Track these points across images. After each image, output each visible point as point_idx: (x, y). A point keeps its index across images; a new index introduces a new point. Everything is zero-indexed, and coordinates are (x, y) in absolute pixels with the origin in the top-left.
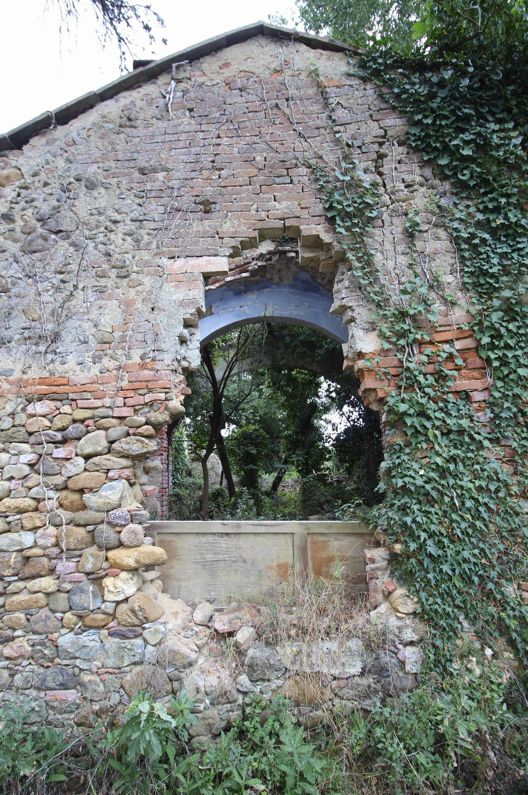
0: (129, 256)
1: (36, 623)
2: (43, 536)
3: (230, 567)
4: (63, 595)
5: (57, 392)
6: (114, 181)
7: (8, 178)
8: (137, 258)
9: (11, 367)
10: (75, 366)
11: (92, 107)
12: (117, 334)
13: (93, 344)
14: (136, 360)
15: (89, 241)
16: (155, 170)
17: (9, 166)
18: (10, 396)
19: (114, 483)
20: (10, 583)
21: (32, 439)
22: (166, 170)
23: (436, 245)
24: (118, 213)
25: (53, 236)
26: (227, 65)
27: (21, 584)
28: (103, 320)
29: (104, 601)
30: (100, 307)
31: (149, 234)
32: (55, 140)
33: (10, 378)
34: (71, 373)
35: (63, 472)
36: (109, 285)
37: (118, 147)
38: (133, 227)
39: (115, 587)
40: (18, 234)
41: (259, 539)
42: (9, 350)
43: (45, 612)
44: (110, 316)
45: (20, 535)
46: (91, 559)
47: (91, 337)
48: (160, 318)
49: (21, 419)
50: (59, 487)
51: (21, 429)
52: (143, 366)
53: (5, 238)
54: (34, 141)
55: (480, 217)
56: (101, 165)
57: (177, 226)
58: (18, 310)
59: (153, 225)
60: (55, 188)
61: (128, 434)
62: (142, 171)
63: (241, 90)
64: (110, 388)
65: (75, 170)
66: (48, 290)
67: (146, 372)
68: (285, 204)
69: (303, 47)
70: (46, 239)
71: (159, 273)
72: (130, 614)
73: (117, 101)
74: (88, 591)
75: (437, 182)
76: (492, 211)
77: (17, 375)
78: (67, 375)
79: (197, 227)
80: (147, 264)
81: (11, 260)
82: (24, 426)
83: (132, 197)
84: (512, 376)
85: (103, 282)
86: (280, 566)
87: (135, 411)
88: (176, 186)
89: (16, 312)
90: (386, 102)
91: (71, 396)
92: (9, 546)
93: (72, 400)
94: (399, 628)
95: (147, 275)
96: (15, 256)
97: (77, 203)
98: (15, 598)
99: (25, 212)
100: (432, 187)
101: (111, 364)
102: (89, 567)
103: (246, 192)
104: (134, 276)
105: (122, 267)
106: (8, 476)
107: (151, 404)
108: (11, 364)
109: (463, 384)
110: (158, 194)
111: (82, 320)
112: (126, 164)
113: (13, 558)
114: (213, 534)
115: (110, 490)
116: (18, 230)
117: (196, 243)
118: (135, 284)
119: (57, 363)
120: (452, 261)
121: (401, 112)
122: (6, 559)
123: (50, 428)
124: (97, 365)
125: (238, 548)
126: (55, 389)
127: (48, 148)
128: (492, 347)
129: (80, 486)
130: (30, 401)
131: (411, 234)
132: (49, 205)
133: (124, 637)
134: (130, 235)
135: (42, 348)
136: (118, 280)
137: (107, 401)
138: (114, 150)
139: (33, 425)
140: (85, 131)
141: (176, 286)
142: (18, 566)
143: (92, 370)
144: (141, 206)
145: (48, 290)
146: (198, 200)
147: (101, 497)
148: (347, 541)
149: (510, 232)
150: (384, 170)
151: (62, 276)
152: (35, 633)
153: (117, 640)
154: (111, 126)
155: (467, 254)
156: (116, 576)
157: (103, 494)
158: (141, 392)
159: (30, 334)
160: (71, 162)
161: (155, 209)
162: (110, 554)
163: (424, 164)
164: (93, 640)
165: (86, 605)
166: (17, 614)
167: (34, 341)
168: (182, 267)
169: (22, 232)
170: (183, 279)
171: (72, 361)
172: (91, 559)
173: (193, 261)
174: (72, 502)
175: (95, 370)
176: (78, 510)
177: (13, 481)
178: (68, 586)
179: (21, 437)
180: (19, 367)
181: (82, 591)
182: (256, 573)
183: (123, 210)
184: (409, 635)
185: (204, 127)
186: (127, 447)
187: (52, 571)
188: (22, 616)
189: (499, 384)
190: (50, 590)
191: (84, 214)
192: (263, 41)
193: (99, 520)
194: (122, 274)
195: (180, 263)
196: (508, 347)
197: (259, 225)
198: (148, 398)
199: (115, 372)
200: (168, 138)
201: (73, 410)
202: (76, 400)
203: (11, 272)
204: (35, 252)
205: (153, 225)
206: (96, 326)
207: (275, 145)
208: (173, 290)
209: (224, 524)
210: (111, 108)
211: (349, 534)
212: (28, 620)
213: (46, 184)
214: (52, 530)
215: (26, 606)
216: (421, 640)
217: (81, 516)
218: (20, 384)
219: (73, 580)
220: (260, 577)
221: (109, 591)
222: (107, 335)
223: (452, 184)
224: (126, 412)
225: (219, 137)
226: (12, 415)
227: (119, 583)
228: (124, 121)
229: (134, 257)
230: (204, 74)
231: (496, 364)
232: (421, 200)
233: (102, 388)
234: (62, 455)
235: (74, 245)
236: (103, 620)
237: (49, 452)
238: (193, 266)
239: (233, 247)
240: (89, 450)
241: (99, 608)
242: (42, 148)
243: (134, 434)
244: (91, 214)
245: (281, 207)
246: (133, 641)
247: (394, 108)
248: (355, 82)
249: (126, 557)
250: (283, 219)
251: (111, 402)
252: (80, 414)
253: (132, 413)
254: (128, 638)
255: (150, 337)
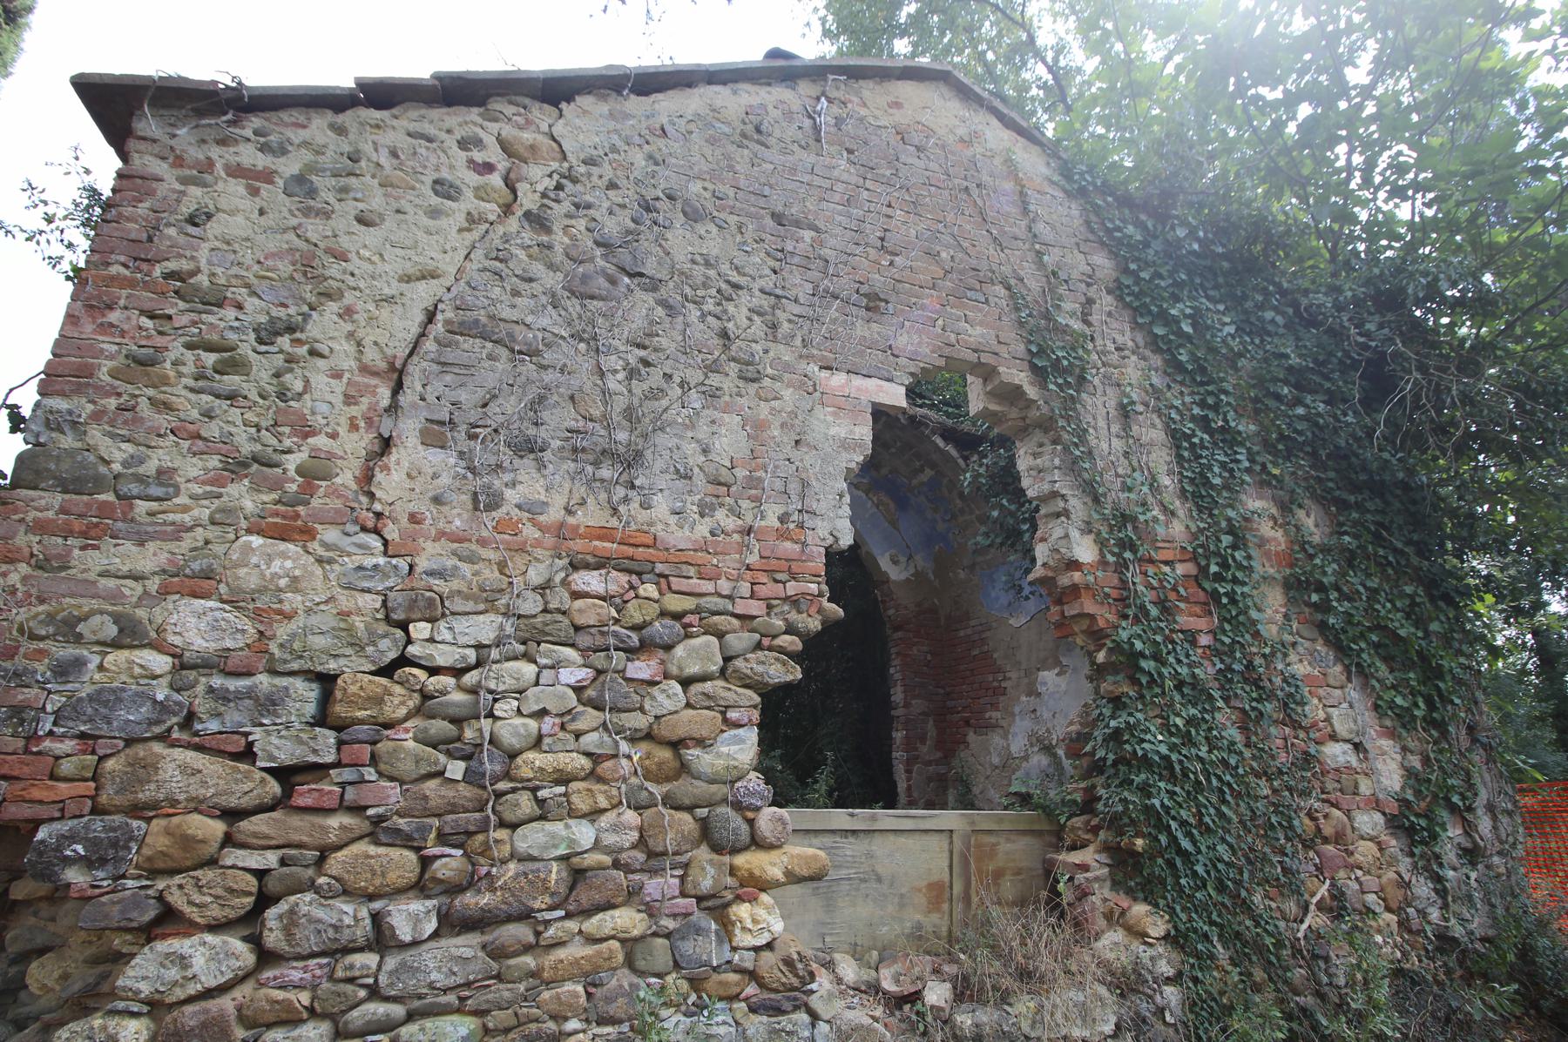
0: (758, 348)
1: (609, 1000)
2: (616, 828)
3: (857, 889)
4: (660, 941)
5: (637, 560)
6: (733, 219)
7: (533, 148)
8: (771, 354)
9: (542, 498)
10: (667, 516)
11: (690, 86)
12: (741, 473)
13: (699, 479)
14: (772, 521)
15: (691, 306)
16: (798, 224)
17: (533, 128)
18: (539, 552)
19: (741, 731)
20: (547, 923)
21: (584, 640)
22: (817, 230)
23: (1152, 432)
24: (739, 273)
25: (626, 280)
26: (897, 105)
27: (572, 925)
28: (717, 445)
29: (734, 949)
30: (713, 422)
31: (790, 321)
32: (627, 116)
33: (541, 518)
34: (660, 527)
35: (647, 707)
36: (725, 387)
37: (738, 167)
38: (765, 303)
39: (755, 921)
40: (558, 256)
41: (902, 840)
42: (541, 466)
43: (625, 978)
44: (729, 442)
45: (567, 826)
46: (708, 872)
47: (696, 470)
48: (808, 459)
49: (559, 598)
50: (639, 735)
51: (559, 617)
52: (783, 535)
53: (530, 256)
54: (585, 101)
55: (1196, 411)
56: (707, 185)
57: (834, 321)
58: (561, 395)
59: (797, 310)
60: (627, 194)
61: (758, 646)
62: (778, 218)
63: (918, 148)
64: (730, 563)
65: (666, 179)
66: (616, 371)
67: (788, 545)
68: (979, 330)
69: (995, 122)
70: (613, 281)
71: (810, 388)
72: (784, 969)
73: (735, 92)
74: (709, 930)
75: (1148, 353)
76: (1210, 407)
77: (554, 514)
78: (653, 530)
79: (861, 330)
80: (788, 368)
81: (544, 299)
82: (564, 613)
83: (763, 255)
84: (1241, 618)
85: (715, 380)
86: (931, 886)
87: (770, 607)
88: (832, 260)
89: (555, 397)
90: (1092, 231)
91: (659, 568)
92: (545, 848)
93: (660, 575)
94: (1152, 958)
95: (788, 386)
96: (553, 295)
97: (669, 235)
98: (561, 953)
99: (573, 222)
100: (1144, 359)
101: (731, 523)
102: (706, 884)
103: (930, 300)
104: (767, 382)
105: (748, 364)
106: (536, 708)
107: (794, 602)
108: (542, 491)
109: (1184, 621)
110: (804, 263)
111: (681, 437)
112: (753, 198)
113: (555, 873)
114: (833, 832)
115: (736, 743)
116: (559, 249)
117: (861, 354)
118: (770, 396)
119: (635, 505)
120: (1168, 459)
121: (1111, 252)
122: (542, 876)
123: (617, 621)
124: (707, 519)
125: (870, 855)
126: (630, 551)
127: (612, 125)
128: (1218, 578)
129: (681, 732)
130: (574, 567)
131: (1125, 412)
132: (619, 224)
133: (778, 1011)
134: (760, 314)
135: (605, 472)
136: (741, 384)
137: (724, 586)
138: (731, 168)
139: (587, 611)
140: (682, 122)
141: (834, 414)
142: (563, 890)
143: (698, 528)
144: (775, 272)
145: (616, 371)
146: (864, 289)
147: (719, 755)
148: (1023, 843)
149: (1228, 437)
150: (1094, 318)
151: (642, 353)
152: (601, 1022)
153: (765, 1019)
154: (727, 130)
155: (1186, 454)
156: (752, 900)
157: (725, 749)
158: (779, 576)
159: (585, 443)
160: (657, 164)
161: (798, 284)
162: (740, 860)
163: (1136, 326)
164: (725, 1023)
165: (705, 957)
166: (569, 987)
167: (591, 458)
168: (842, 386)
169: (567, 255)
170: (843, 405)
171: (661, 506)
172: (708, 872)
173: (858, 381)
174: (660, 764)
175: (703, 529)
176: (676, 777)
177: (547, 719)
178: (671, 924)
179: (562, 634)
180: (559, 501)
181: (699, 931)
182: (896, 900)
183: (747, 270)
184: (1165, 969)
185: (869, 184)
186: (760, 669)
187: (633, 895)
188: (580, 989)
189: (1227, 627)
190: (636, 933)
191: (682, 258)
192: (944, 89)
193: (719, 797)
194: (749, 375)
195: (838, 380)
196: (1235, 581)
197: (947, 351)
198: (792, 588)
199: (736, 536)
200: (817, 181)
201: (661, 593)
202: (666, 577)
203: (544, 322)
204: (592, 297)
205: (797, 310)
206: (705, 451)
207: (966, 244)
208: (830, 418)
209: (852, 815)
210: (733, 101)
211: (1024, 832)
212: (589, 995)
213: (612, 186)
214: (631, 817)
215: (589, 968)
216: (1180, 974)
217: (685, 788)
218: (561, 532)
219: (677, 911)
220: (902, 906)
221: (744, 929)
222: (724, 471)
223: (1166, 361)
224: (756, 608)
225: (889, 206)
226: (544, 588)
227: (761, 913)
228: (749, 129)
229: (766, 352)
230: (865, 105)
231: (1225, 600)
232: (1133, 371)
233: (715, 561)
234: (645, 674)
235: (663, 303)
236: (737, 984)
237: (620, 667)
238: (858, 389)
239: (912, 374)
240: (693, 669)
241: (728, 962)
242: (601, 121)
243: (770, 649)
244: (693, 262)
245: (977, 334)
246: (794, 1016)
247: (1103, 244)
248: (1059, 194)
249: (770, 865)
250: (975, 351)
251: (725, 585)
252: (675, 603)
253: (765, 611)
254: (784, 1013)
255: (794, 487)
